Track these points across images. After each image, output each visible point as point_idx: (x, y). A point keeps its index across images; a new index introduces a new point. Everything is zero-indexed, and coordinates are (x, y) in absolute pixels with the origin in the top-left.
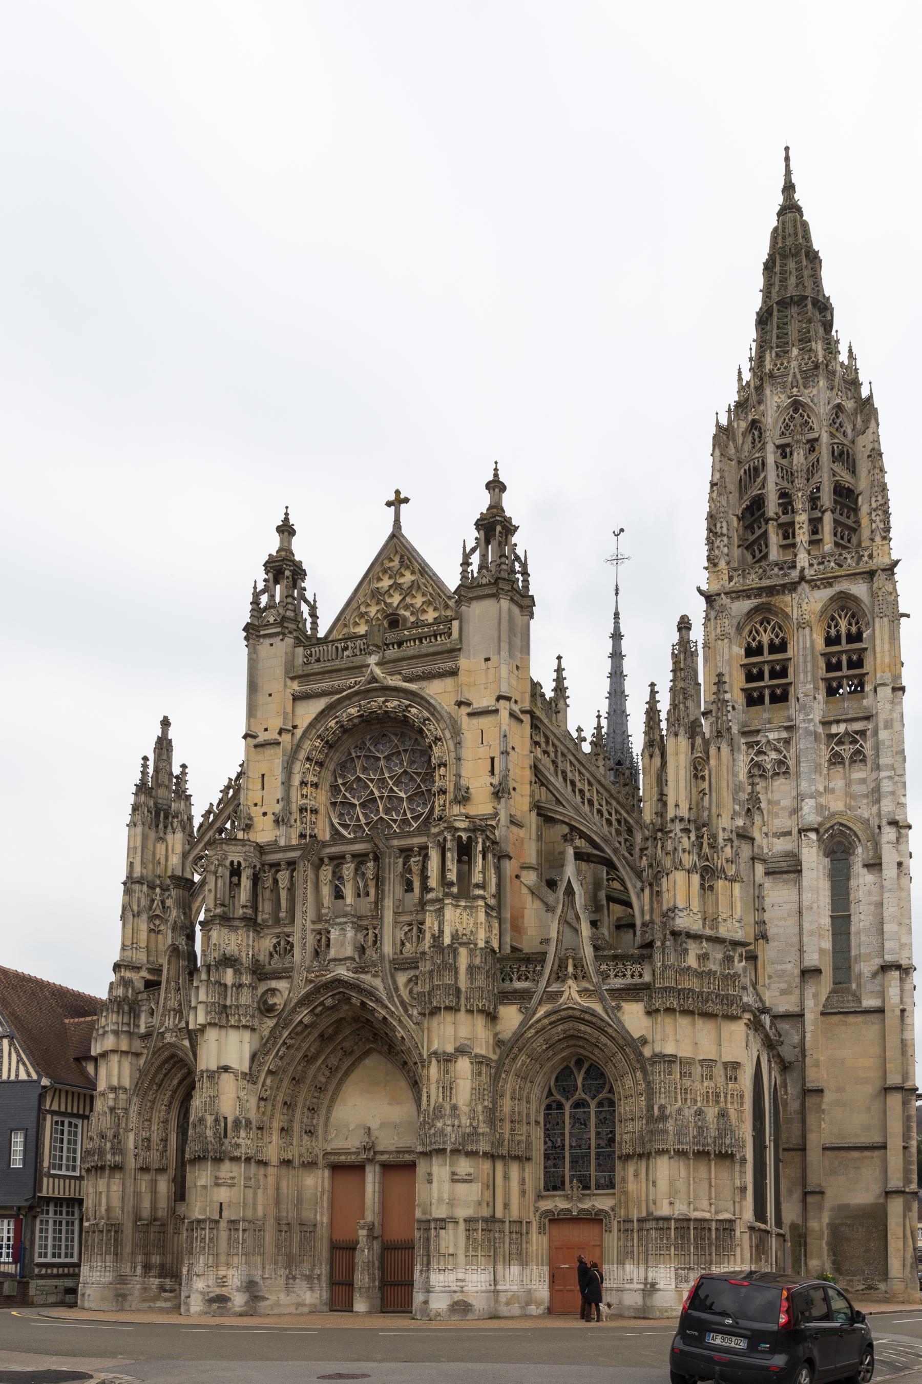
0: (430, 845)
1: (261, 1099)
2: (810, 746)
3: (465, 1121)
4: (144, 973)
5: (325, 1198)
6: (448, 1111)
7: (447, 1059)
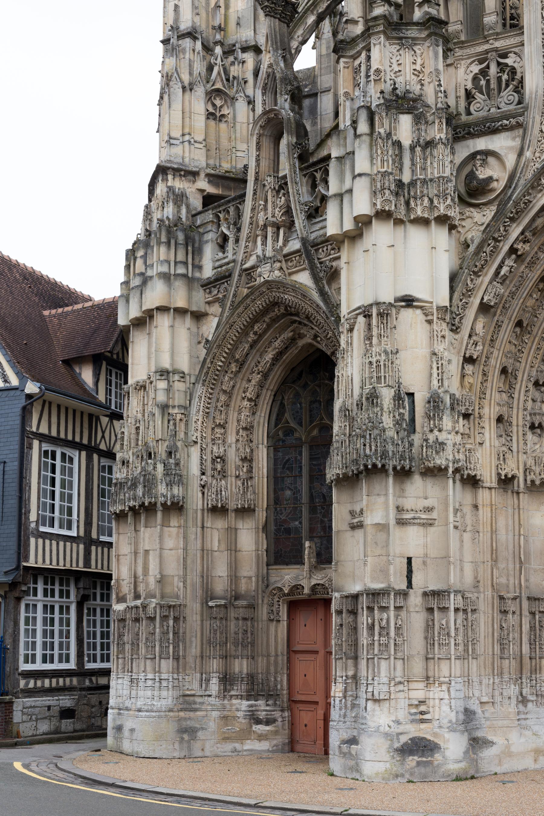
1: (469, 360)
4: (203, 184)
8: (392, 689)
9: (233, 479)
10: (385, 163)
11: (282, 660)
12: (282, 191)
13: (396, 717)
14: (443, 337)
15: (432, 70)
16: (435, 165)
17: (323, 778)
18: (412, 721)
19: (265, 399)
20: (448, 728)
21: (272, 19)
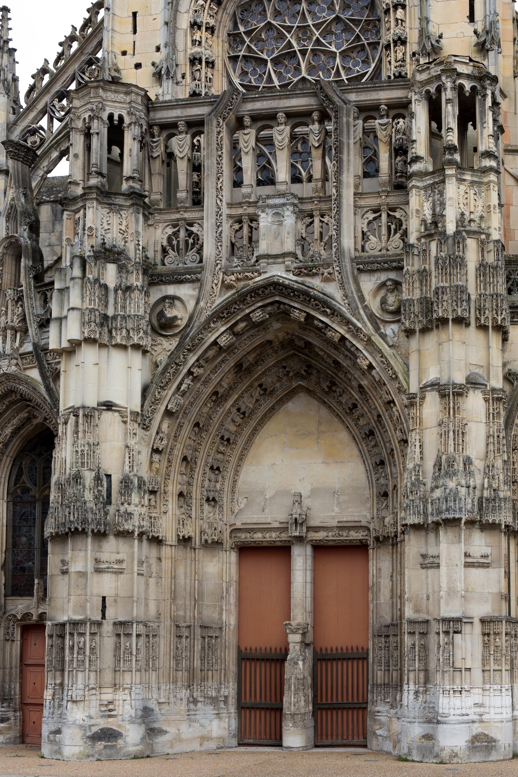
0: (414, 98)
1: (156, 451)
3: (478, 480)
5: (233, 591)
6: (461, 467)
8: (86, 693)
10: (93, 302)
11: (16, 671)
12: (20, 303)
13: (89, 713)
14: (135, 434)
15: (134, 231)
16: (132, 305)
17: (38, 760)
18: (102, 716)
19: (5, 463)
20: (129, 721)
21: (16, 161)
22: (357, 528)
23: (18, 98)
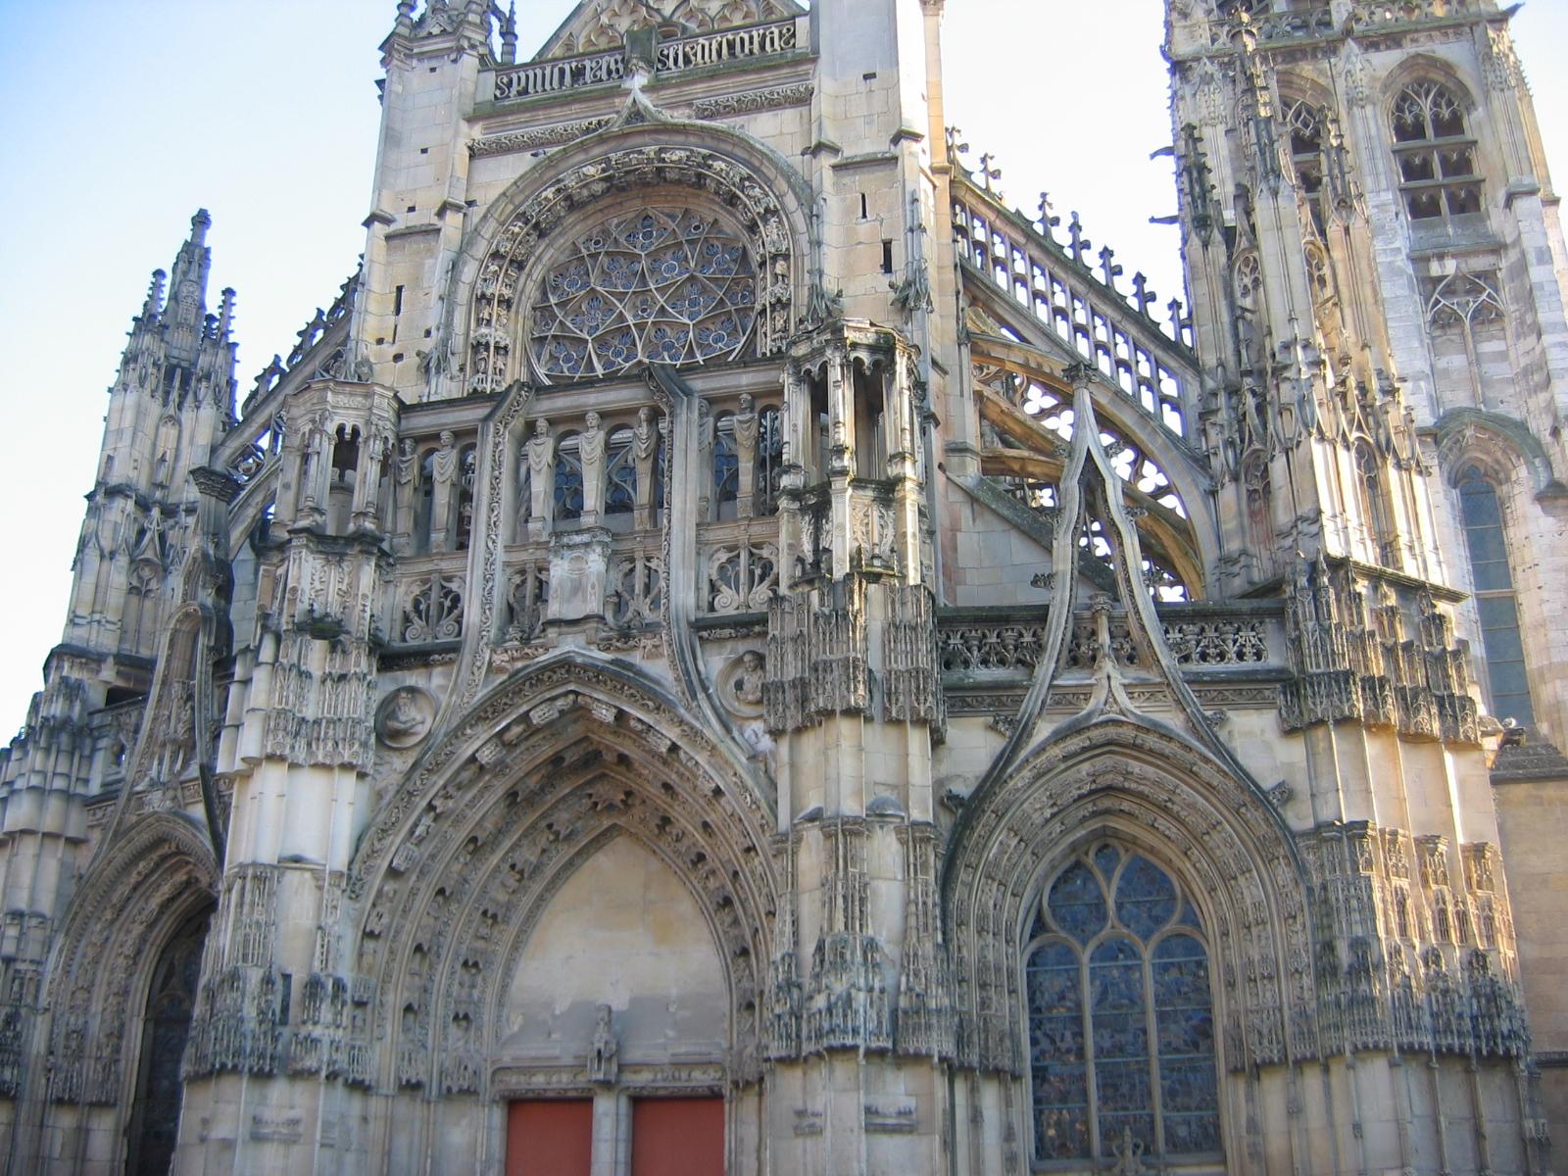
2: (1399, 292)
7: (845, 832)
9: (93, 1062)
22: (705, 1064)
23: (233, 409)
